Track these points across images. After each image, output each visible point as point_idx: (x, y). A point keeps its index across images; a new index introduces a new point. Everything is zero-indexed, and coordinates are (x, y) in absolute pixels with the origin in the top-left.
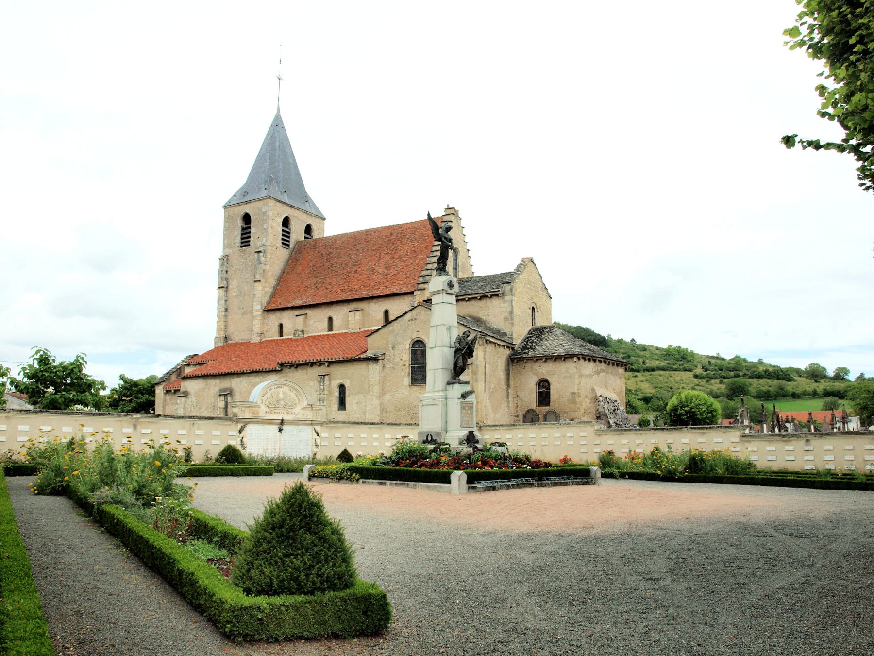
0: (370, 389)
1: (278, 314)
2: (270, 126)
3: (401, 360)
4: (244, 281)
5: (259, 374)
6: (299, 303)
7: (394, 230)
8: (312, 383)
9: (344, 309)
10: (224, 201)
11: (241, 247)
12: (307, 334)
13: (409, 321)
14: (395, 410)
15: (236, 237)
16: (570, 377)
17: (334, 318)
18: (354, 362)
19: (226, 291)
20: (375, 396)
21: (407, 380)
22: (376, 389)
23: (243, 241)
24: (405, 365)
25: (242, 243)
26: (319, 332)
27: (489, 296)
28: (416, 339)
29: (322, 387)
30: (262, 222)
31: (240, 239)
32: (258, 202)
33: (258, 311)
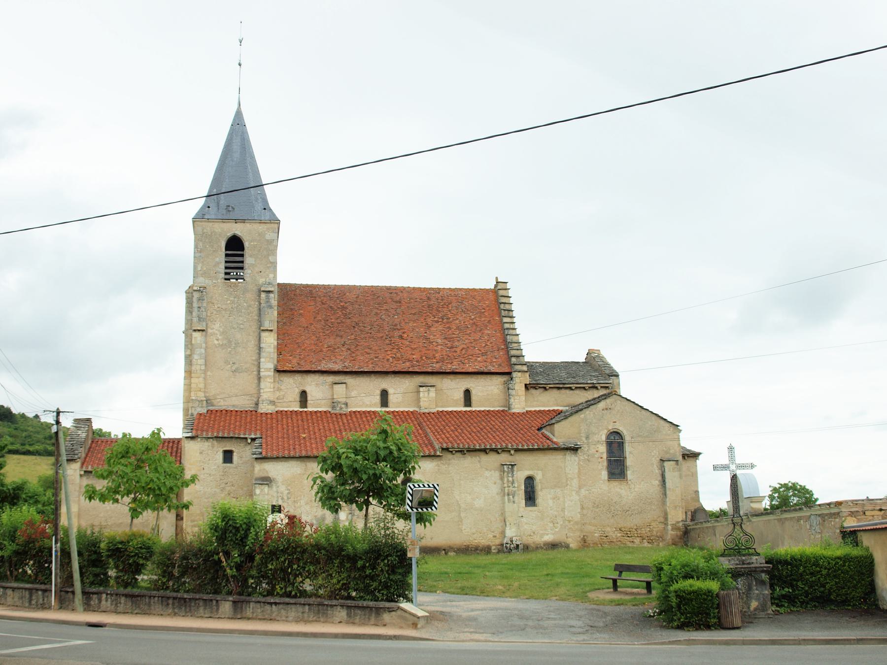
0: (569, 482)
1: (298, 378)
3: (597, 451)
6: (336, 367)
7: (430, 294)
8: (487, 474)
13: (603, 410)
14: (593, 507)
15: (218, 263)
16: (693, 476)
18: (546, 451)
19: (206, 336)
20: (574, 490)
21: (604, 474)
22: (575, 483)
24: (601, 458)
26: (370, 406)
27: (599, 388)
28: (612, 431)
29: (510, 479)
30: (265, 253)
31: (224, 268)
33: (268, 370)
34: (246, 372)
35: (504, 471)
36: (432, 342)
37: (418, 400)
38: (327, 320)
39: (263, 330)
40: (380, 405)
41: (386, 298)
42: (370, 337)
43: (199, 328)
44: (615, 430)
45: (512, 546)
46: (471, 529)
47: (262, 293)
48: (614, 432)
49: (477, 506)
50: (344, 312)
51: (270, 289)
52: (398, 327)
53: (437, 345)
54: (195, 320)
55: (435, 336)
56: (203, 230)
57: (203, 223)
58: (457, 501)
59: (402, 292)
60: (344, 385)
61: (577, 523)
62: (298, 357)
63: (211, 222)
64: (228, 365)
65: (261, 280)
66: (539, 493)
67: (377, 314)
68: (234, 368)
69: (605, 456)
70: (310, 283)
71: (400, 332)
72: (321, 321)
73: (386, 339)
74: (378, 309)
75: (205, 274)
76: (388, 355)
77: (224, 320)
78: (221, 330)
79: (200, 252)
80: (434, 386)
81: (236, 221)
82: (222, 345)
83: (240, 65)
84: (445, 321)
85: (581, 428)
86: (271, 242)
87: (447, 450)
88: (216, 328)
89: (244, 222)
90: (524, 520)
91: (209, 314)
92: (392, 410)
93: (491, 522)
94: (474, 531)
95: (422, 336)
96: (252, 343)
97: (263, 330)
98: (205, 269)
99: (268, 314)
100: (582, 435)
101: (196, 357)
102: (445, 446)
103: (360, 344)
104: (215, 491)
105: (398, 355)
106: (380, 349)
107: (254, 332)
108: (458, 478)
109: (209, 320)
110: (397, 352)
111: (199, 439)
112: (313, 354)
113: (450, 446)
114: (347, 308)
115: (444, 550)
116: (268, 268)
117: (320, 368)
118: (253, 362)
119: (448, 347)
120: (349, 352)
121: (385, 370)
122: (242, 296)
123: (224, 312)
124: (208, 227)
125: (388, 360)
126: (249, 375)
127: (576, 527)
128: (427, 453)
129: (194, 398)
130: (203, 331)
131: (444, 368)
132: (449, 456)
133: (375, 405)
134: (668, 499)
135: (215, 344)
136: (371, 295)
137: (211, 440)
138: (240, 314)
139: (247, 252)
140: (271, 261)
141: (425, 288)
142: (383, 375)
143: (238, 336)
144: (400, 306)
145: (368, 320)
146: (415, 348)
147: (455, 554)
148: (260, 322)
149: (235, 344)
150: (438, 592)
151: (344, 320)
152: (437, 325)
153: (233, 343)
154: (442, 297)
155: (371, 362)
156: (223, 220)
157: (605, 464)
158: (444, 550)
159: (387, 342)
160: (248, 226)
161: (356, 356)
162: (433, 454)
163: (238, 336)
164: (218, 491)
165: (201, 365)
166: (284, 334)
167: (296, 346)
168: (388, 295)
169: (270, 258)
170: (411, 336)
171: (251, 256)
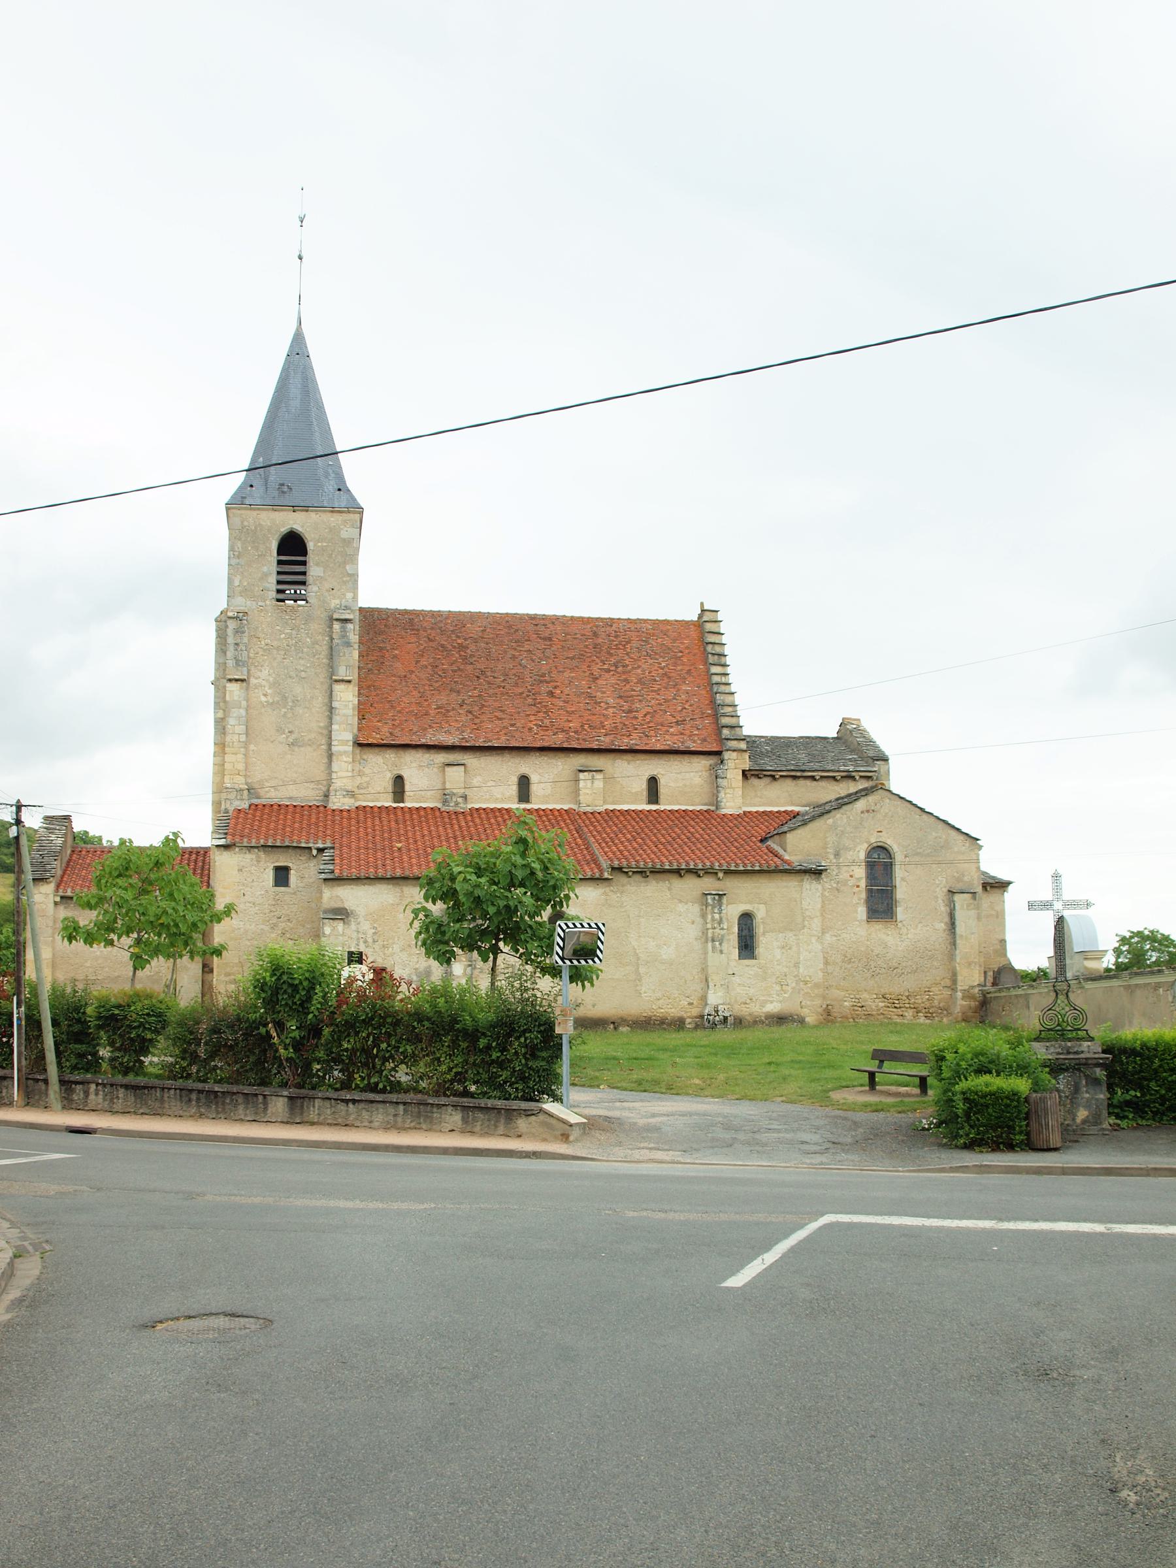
1: (390, 755)
2: (286, 355)
3: (851, 876)
4: (293, 674)
6: (450, 740)
7: (597, 627)
8: (681, 907)
9: (561, 766)
11: (278, 600)
12: (472, 802)
13: (862, 812)
15: (265, 576)
16: (997, 917)
17: (534, 778)
19: (247, 689)
21: (862, 911)
22: (816, 924)
24: (858, 886)
26: (502, 801)
28: (875, 845)
30: (340, 559)
31: (275, 582)
32: (329, 514)
33: (345, 743)
34: (309, 745)
35: (707, 905)
36: (600, 703)
37: (577, 791)
39: (336, 681)
40: (516, 800)
42: (502, 694)
43: (237, 677)
44: (879, 844)
45: (717, 1018)
46: (654, 991)
47: (335, 622)
48: (878, 847)
49: (664, 957)
50: (463, 653)
52: (547, 678)
54: (231, 663)
55: (604, 693)
56: (242, 522)
57: (242, 512)
58: (634, 949)
59: (553, 623)
61: (817, 986)
63: (254, 509)
66: (761, 938)
67: (514, 657)
69: (863, 884)
70: (410, 607)
71: (550, 685)
73: (528, 696)
74: (515, 649)
75: (246, 592)
77: (275, 664)
78: (271, 679)
81: (295, 508)
83: (300, 258)
84: (620, 669)
85: (828, 839)
86: (349, 542)
87: (620, 869)
88: (263, 676)
89: (307, 511)
90: (736, 979)
92: (536, 807)
93: (686, 981)
94: (659, 995)
95: (583, 693)
96: (320, 701)
97: (336, 681)
98: (245, 584)
99: (344, 655)
100: (828, 850)
101: (232, 721)
102: (616, 864)
104: (262, 929)
105: (547, 722)
106: (519, 713)
107: (322, 683)
111: (237, 849)
113: (625, 864)
115: (614, 1023)
116: (345, 583)
118: (320, 730)
120: (470, 716)
123: (275, 652)
124: (251, 517)
125: (530, 729)
126: (315, 750)
127: (816, 991)
129: (229, 785)
130: (242, 680)
132: (623, 879)
133: (509, 799)
134: (957, 952)
137: (256, 850)
138: (300, 655)
139: (311, 558)
141: (589, 618)
143: (298, 690)
145: (500, 667)
146: (573, 712)
149: (293, 702)
153: (289, 700)
155: (503, 732)
156: (275, 507)
157: (864, 895)
158: (614, 1023)
160: (313, 516)
161: (481, 722)
162: (597, 875)
163: (298, 690)
164: (267, 928)
166: (369, 687)
168: (531, 628)
169: (348, 567)
170: (567, 692)
171: (317, 565)
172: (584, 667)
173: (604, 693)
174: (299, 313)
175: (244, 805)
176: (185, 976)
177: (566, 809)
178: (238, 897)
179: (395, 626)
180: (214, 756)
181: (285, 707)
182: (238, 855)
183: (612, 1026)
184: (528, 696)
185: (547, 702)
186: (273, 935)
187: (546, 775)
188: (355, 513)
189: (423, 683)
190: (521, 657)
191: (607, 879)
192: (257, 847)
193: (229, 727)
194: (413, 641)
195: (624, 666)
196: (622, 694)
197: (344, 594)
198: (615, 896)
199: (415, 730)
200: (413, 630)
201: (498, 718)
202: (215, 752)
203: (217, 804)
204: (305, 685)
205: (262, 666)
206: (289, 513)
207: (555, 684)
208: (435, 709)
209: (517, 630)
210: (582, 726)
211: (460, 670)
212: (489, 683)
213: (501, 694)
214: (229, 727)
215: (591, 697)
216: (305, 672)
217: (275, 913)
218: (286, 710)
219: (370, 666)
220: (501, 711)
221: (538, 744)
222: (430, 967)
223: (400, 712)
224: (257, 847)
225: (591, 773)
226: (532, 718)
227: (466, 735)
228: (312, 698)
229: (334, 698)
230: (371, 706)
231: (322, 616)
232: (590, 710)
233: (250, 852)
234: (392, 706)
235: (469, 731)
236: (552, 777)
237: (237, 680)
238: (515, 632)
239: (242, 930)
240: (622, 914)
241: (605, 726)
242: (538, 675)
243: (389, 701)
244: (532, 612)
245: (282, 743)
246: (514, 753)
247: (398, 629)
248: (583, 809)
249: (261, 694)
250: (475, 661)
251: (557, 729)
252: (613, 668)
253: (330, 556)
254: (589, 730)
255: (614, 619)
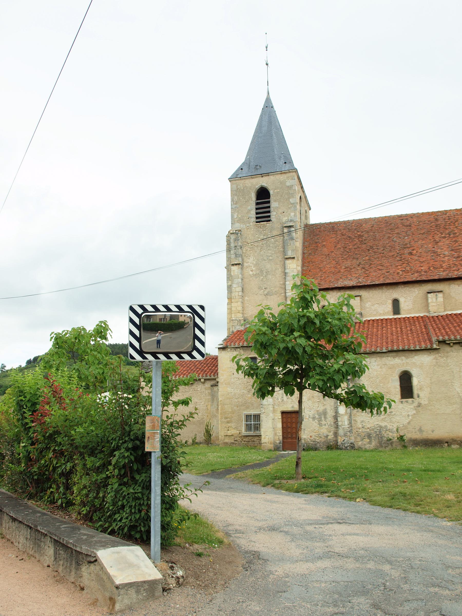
4: (265, 258)
5: (400, 353)
6: (351, 284)
7: (437, 216)
10: (230, 173)
11: (257, 222)
12: (366, 317)
15: (250, 211)
17: (402, 300)
19: (242, 269)
23: (268, 214)
25: (257, 218)
26: (384, 314)
30: (286, 196)
31: (255, 213)
32: (280, 175)
34: (276, 294)
36: (440, 255)
37: (427, 305)
38: (346, 247)
39: (287, 259)
40: (392, 313)
41: (397, 224)
42: (382, 257)
43: (236, 263)
47: (285, 228)
50: (361, 239)
51: (291, 224)
52: (408, 246)
53: (445, 257)
54: (233, 256)
55: (442, 249)
56: (237, 186)
57: (237, 181)
58: (458, 393)
59: (412, 217)
60: (359, 298)
62: (319, 278)
63: (242, 179)
64: (261, 290)
65: (284, 218)
67: (389, 238)
68: (266, 292)
70: (332, 221)
71: (410, 249)
72: (340, 248)
73: (397, 256)
74: (390, 233)
75: (240, 220)
76: (398, 269)
77: (256, 255)
78: (255, 262)
79: (236, 204)
80: (441, 291)
81: (262, 175)
82: (255, 275)
83: (267, 64)
84: (452, 236)
86: (291, 187)
87: (443, 342)
88: (250, 262)
89: (269, 175)
91: (244, 251)
92: (404, 316)
95: (430, 251)
96: (279, 271)
97: (287, 259)
98: (240, 216)
99: (290, 245)
101: (234, 286)
102: (441, 338)
103: (373, 263)
104: (243, 392)
105: (408, 268)
106: (392, 265)
107: (280, 261)
108: (458, 370)
109: (245, 256)
110: (407, 266)
111: (229, 350)
112: (332, 275)
113: (446, 338)
114: (363, 236)
115: (447, 442)
116: (290, 208)
117: (337, 285)
118: (281, 286)
119: (454, 257)
120: (364, 270)
121: (394, 281)
122: (269, 233)
123: (256, 248)
124: (241, 183)
125: (398, 273)
126: (278, 296)
128: (423, 346)
129: (234, 319)
130: (239, 264)
131: (450, 275)
132: (447, 348)
133: (388, 313)
135: (250, 275)
136: (384, 223)
137: (239, 349)
138: (269, 248)
139: (272, 199)
140: (292, 202)
141: (432, 212)
142: (394, 287)
143: (268, 266)
144: (410, 229)
145: (381, 243)
146: (424, 261)
147: (458, 446)
148: (284, 252)
149: (266, 272)
150: (358, 500)
151: (360, 246)
152: (444, 240)
153: (264, 272)
154: (449, 217)
155: (382, 276)
156: (252, 176)
158: (447, 442)
159: (398, 258)
160: (272, 178)
161: (370, 273)
162: (429, 347)
163: (268, 266)
164: (245, 392)
165: (239, 292)
166: (309, 262)
167: (318, 270)
168: (399, 222)
169: (291, 200)
170: (420, 252)
171: (275, 201)
172: (430, 237)
173: (442, 249)
174: (268, 89)
175: (242, 328)
176: (215, 420)
177: (422, 316)
178: (230, 375)
179: (324, 231)
180: (228, 305)
181: (262, 276)
182: (229, 353)
183: (446, 445)
184: (397, 256)
185: (408, 258)
186: (249, 396)
187: (409, 298)
188: (293, 172)
189: (338, 256)
190: (393, 237)
191: (436, 349)
192: (239, 348)
193: (233, 288)
194: (333, 236)
195: (454, 234)
196: (453, 249)
197: (290, 214)
198: (442, 360)
199: (332, 280)
200: (334, 231)
201: (379, 270)
202: (228, 303)
203: (229, 329)
204: (272, 263)
205: (250, 256)
206: (260, 178)
207: (413, 248)
208: (344, 269)
209: (391, 224)
210: (429, 268)
211: (358, 247)
212: (375, 252)
213: (381, 257)
214: (233, 288)
215: (434, 252)
216: (272, 256)
217: (250, 383)
218: (263, 277)
219: (310, 252)
220: (381, 265)
221: (402, 280)
222: (326, 409)
223: (324, 272)
224: (239, 348)
225: (435, 294)
226: (399, 267)
227: (360, 280)
228: (276, 269)
229: (286, 268)
230: (309, 271)
231: (279, 227)
232: (434, 259)
233: (235, 350)
234: (321, 270)
235: (362, 278)
236: (412, 298)
237: (236, 264)
238: (390, 225)
239: (233, 393)
240: (448, 371)
241: (443, 267)
242: (403, 245)
243: (320, 268)
244: (399, 214)
245: (261, 295)
246: (389, 287)
247: (326, 232)
248: (432, 315)
249: (250, 270)
250: (367, 242)
251: (414, 271)
252: (448, 236)
253: (281, 196)
254: (433, 270)
255: (447, 210)
